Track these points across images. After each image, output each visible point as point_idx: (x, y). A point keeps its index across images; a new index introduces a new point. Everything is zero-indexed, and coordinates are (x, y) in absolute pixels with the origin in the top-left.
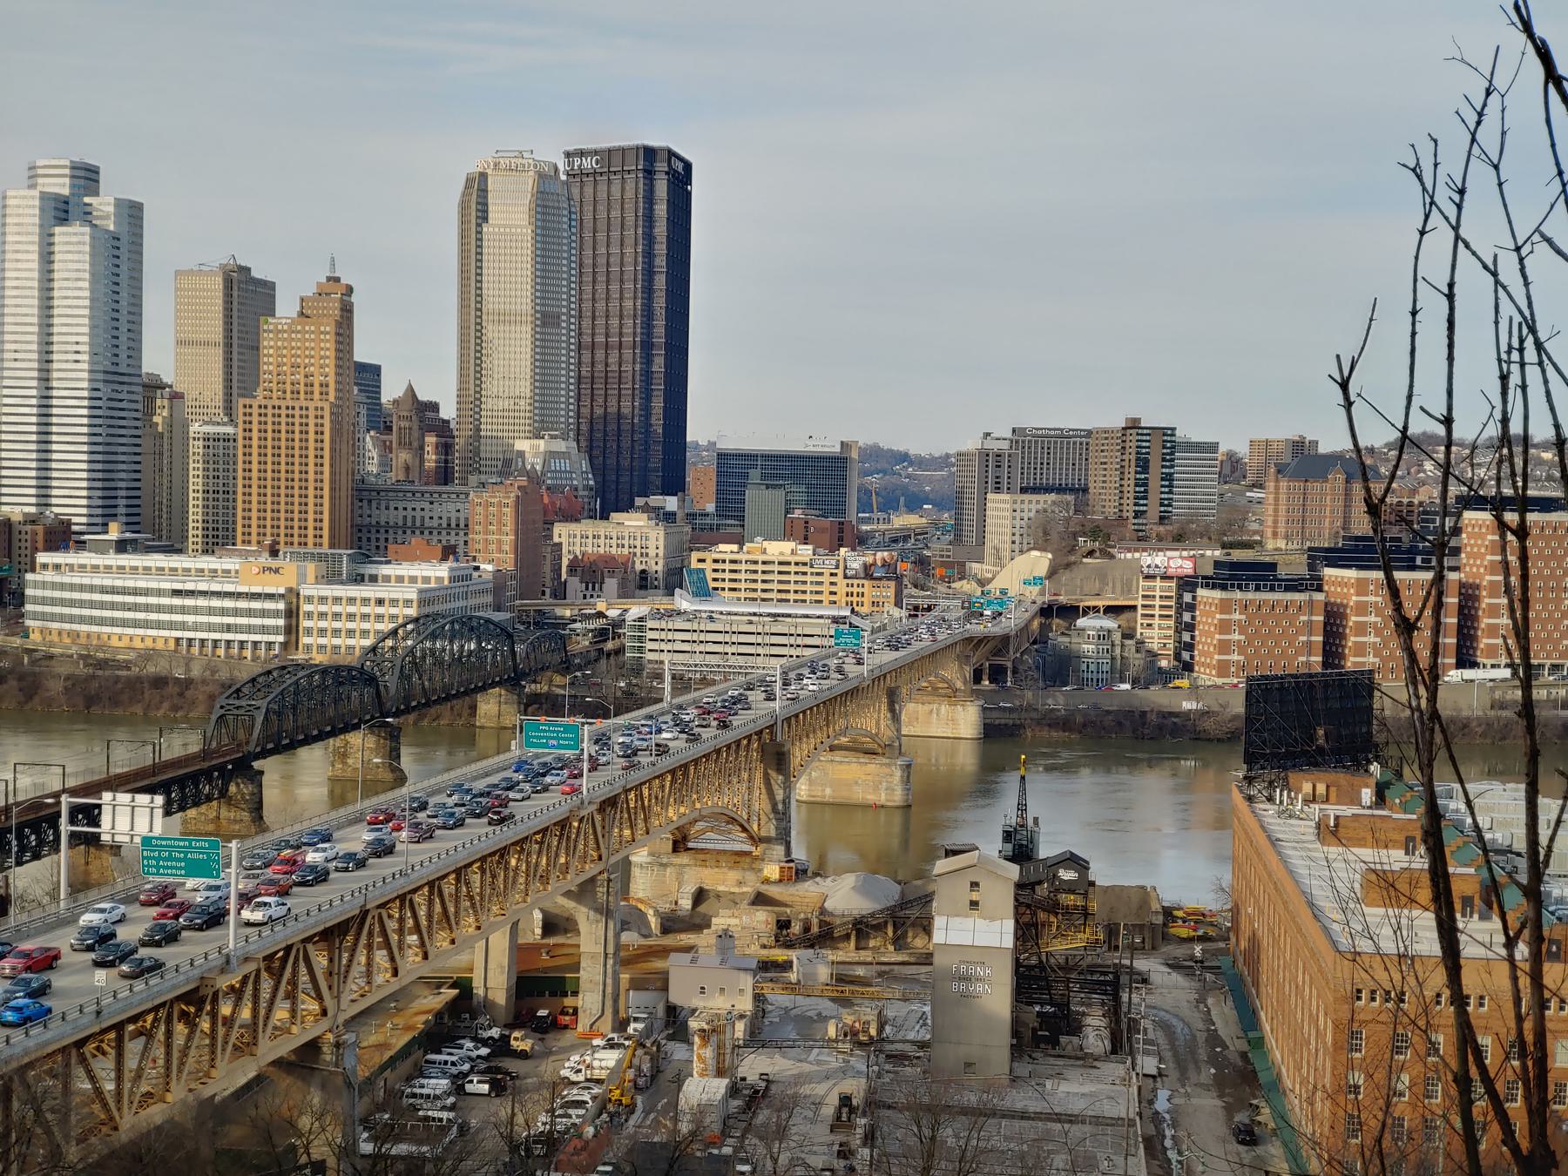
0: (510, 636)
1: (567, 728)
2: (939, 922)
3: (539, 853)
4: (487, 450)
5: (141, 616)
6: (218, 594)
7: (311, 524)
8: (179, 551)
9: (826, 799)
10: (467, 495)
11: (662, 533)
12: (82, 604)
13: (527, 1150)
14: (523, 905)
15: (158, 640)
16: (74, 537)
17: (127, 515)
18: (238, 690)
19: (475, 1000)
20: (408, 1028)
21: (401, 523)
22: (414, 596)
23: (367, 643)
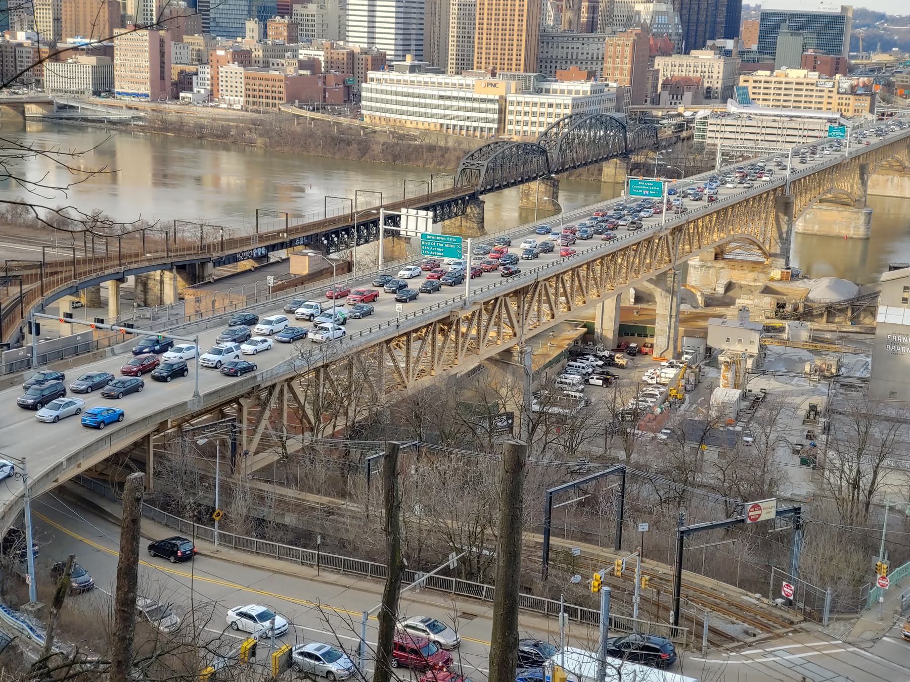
0: (624, 127)
1: (655, 184)
2: (881, 309)
3: (635, 257)
5: (422, 110)
6: (463, 99)
7: (514, 57)
8: (443, 73)
9: (814, 232)
10: (604, 39)
11: (722, 63)
12: (391, 102)
13: (622, 417)
14: (624, 285)
15: (425, 123)
16: (388, 63)
17: (416, 50)
18: (472, 155)
19: (596, 335)
20: (559, 347)
22: (569, 102)
23: (543, 129)
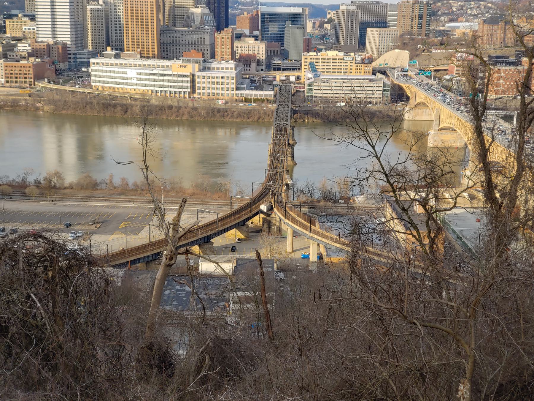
4: (178, 12)
11: (264, 46)
21: (172, 42)
